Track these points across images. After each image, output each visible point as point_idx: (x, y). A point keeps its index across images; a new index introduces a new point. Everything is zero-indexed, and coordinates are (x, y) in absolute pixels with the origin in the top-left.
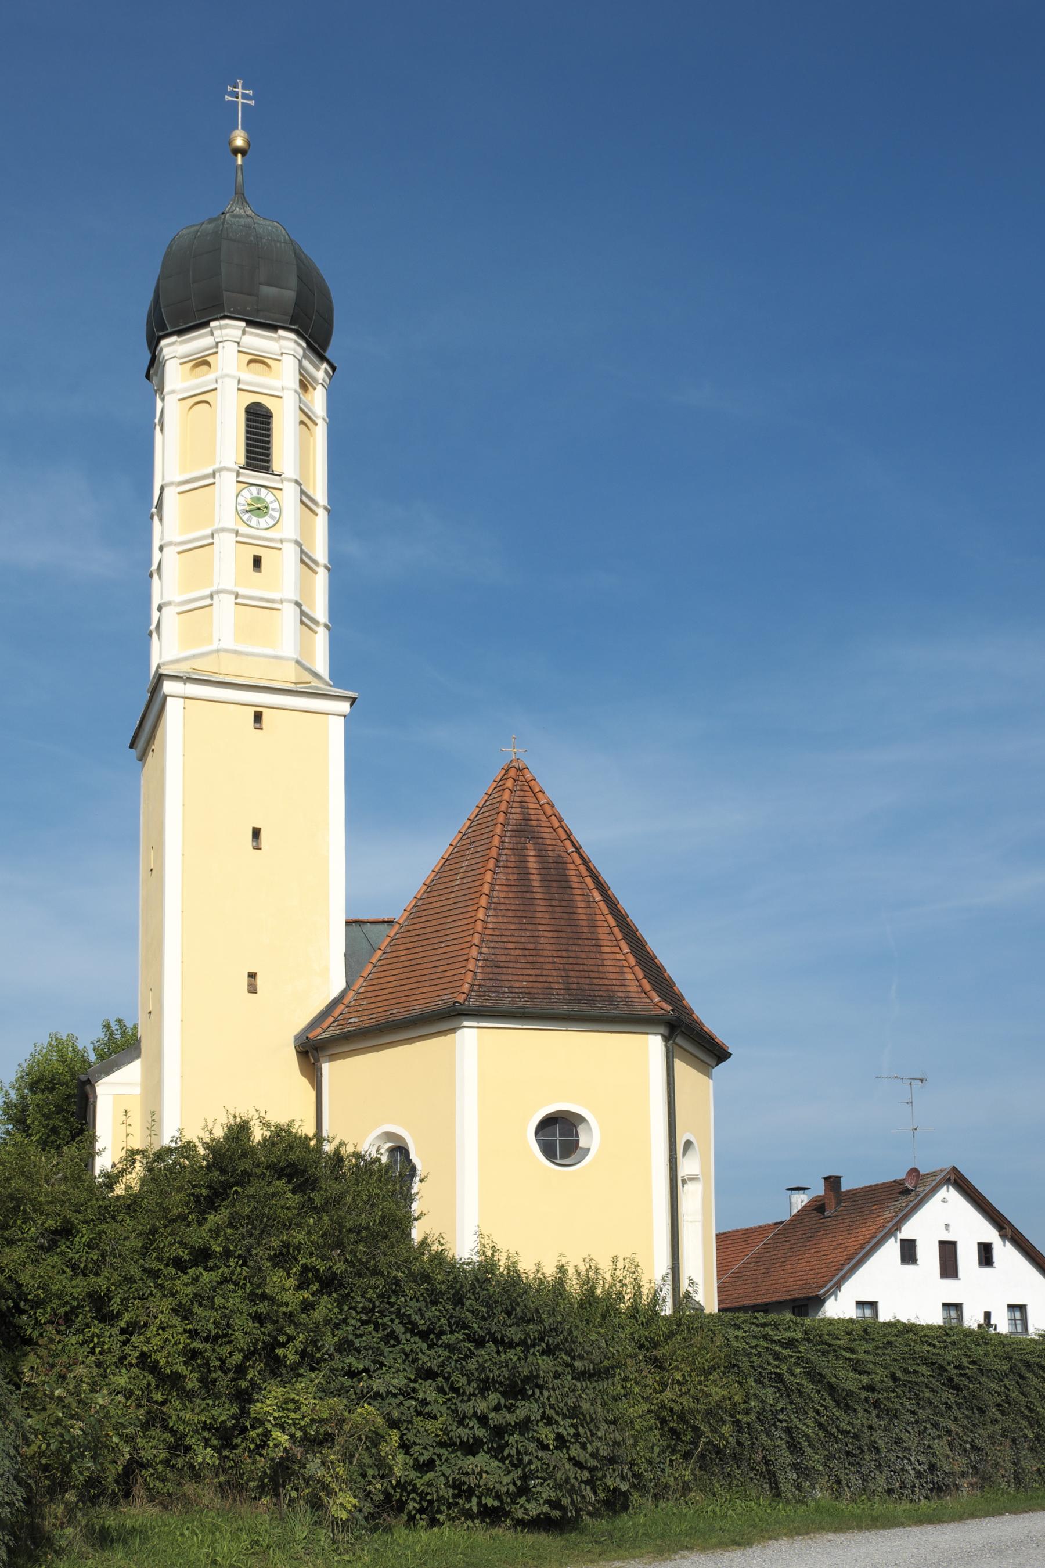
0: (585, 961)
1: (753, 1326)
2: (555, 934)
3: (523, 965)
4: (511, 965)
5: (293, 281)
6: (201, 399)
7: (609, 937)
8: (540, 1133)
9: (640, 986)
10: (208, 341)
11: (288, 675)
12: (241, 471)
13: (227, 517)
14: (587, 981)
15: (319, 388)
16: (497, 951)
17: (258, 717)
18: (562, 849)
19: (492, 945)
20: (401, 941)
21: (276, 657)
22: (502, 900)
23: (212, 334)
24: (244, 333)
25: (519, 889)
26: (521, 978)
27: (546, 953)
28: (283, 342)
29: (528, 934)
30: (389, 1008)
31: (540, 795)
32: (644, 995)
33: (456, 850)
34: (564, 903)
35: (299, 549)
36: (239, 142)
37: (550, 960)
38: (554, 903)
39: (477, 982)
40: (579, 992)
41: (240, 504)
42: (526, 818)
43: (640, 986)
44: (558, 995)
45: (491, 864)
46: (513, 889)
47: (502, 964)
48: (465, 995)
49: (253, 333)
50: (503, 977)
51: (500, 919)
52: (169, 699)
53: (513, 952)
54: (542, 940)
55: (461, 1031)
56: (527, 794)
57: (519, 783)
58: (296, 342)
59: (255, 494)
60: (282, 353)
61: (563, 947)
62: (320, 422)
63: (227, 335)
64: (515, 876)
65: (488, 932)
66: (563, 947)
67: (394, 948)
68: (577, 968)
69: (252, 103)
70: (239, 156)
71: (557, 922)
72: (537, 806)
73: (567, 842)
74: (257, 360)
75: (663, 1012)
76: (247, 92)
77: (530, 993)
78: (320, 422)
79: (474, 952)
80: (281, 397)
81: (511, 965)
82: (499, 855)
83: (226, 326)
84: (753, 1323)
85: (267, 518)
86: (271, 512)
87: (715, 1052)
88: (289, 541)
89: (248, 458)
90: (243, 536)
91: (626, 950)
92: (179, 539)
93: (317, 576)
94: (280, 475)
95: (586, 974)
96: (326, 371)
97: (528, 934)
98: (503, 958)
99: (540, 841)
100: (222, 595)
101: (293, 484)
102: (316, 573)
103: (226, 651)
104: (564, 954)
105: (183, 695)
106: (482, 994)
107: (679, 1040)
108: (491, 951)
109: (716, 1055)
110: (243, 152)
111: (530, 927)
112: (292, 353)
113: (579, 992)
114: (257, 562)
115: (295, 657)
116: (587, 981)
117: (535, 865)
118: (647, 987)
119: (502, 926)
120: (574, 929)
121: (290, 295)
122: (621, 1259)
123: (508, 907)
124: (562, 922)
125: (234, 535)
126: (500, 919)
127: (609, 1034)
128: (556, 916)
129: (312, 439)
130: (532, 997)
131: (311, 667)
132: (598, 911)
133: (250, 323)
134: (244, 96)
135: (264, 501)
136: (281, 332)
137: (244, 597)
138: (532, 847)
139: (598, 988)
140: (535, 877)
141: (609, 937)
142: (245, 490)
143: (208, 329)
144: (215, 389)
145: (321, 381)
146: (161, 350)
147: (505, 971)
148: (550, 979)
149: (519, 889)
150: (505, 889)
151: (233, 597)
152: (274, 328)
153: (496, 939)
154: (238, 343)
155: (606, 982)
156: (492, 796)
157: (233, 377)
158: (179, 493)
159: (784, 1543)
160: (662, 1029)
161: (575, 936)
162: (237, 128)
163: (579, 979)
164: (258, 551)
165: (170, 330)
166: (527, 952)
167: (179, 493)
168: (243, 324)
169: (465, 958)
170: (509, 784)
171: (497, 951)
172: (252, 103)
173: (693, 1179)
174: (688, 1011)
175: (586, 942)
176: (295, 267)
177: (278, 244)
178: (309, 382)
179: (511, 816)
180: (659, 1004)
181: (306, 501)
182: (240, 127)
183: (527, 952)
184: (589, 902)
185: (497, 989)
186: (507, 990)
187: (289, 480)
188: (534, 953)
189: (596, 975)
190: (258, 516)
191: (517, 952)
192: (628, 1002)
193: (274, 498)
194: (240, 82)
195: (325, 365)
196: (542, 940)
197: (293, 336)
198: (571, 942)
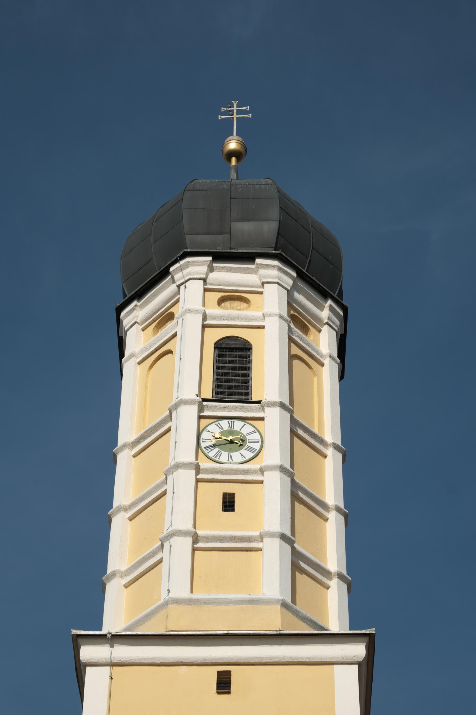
5: (275, 213)
12: (205, 403)
15: (325, 329)
21: (251, 602)
23: (174, 282)
24: (211, 269)
28: (262, 272)
35: (289, 480)
36: (233, 145)
41: (204, 440)
49: (223, 268)
58: (280, 269)
60: (263, 284)
62: (327, 361)
70: (234, 159)
78: (327, 361)
80: (263, 327)
83: (188, 263)
85: (243, 451)
86: (248, 444)
90: (207, 471)
92: (127, 502)
93: (328, 524)
96: (331, 309)
101: (277, 410)
102: (326, 520)
103: (177, 601)
105: (108, 661)
112: (276, 280)
115: (281, 598)
129: (315, 379)
135: (237, 433)
136: (258, 261)
137: (208, 539)
142: (213, 425)
143: (170, 276)
144: (175, 335)
145: (326, 321)
151: (189, 540)
154: (205, 280)
157: (197, 311)
159: (218, 416)
162: (232, 135)
164: (229, 488)
165: (128, 296)
168: (210, 258)
187: (272, 404)
193: (253, 429)
195: (330, 302)
197: (275, 263)
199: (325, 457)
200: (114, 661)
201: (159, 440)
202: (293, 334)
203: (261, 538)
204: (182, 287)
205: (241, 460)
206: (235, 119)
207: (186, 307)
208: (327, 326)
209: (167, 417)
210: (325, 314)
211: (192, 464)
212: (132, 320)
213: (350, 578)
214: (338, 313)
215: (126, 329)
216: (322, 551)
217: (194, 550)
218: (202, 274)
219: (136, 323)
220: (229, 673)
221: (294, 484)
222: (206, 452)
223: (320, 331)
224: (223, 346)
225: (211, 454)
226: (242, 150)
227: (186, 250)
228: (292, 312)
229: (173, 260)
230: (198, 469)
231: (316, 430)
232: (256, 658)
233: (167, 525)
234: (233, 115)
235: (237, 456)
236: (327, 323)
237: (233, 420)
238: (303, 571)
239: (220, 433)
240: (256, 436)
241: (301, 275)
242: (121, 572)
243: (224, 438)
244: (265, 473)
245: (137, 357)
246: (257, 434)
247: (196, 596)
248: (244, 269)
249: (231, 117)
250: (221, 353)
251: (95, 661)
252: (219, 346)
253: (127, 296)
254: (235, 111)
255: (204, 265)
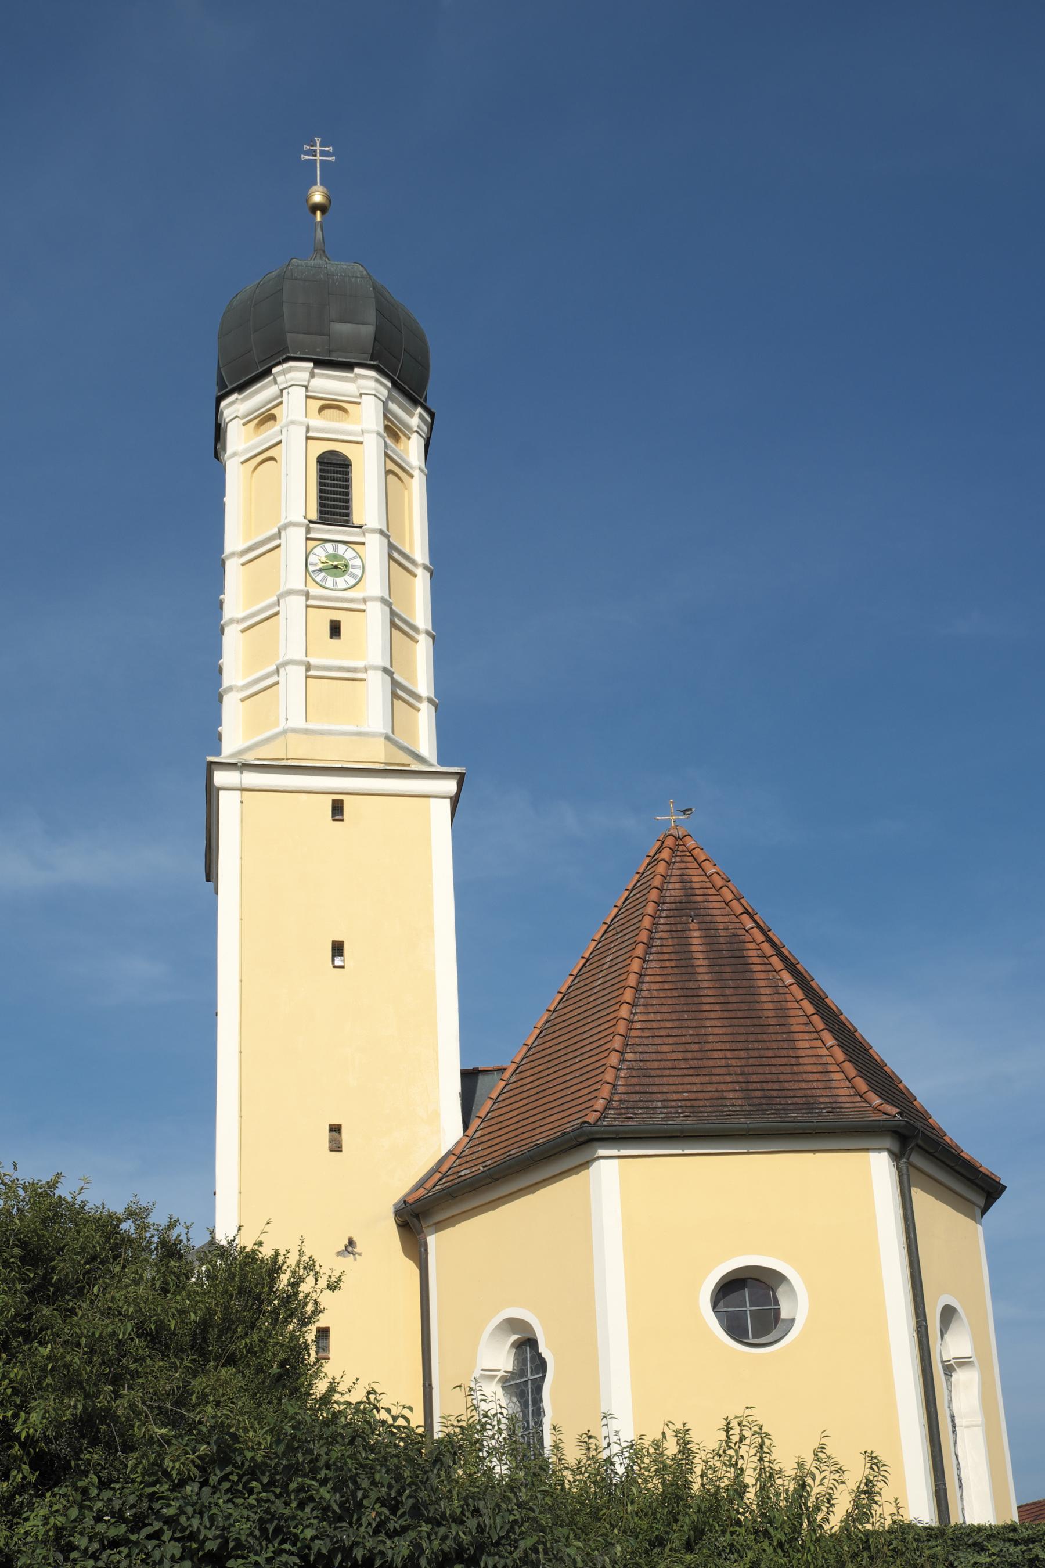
0: (773, 1061)
1: (1007, 1545)
2: (729, 1030)
3: (685, 1072)
4: (667, 1072)
5: (372, 316)
6: (265, 457)
7: (807, 1029)
8: (721, 1304)
9: (853, 1087)
10: (273, 390)
11: (376, 754)
12: (312, 525)
13: (296, 579)
14: (776, 1086)
15: (414, 436)
16: (647, 1057)
17: (338, 809)
18: (738, 926)
19: (639, 1049)
20: (528, 1066)
21: (360, 734)
22: (655, 993)
23: (275, 382)
24: (312, 375)
25: (678, 978)
26: (680, 1088)
27: (715, 1055)
28: (361, 382)
29: (691, 1032)
30: (507, 1149)
31: (706, 865)
32: (858, 1099)
33: (599, 945)
34: (741, 991)
35: (387, 610)
36: (318, 198)
37: (723, 1062)
38: (728, 992)
39: (616, 1097)
40: (763, 1101)
41: (312, 564)
42: (688, 892)
43: (853, 1087)
44: (734, 1106)
45: (640, 950)
46: (670, 978)
47: (654, 1073)
48: (598, 1114)
49: (323, 375)
50: (655, 1089)
51: (652, 1017)
52: (221, 793)
53: (669, 1056)
54: (711, 1038)
55: (596, 1164)
56: (689, 865)
57: (679, 853)
58: (377, 380)
59: (331, 551)
60: (361, 395)
61: (741, 1045)
62: (416, 473)
63: (292, 379)
64: (673, 964)
65: (633, 1033)
66: (741, 1045)
67: (520, 1076)
68: (760, 1070)
69: (333, 159)
70: (318, 213)
71: (732, 1014)
72: (704, 878)
73: (745, 917)
74: (331, 406)
75: (885, 1116)
76: (327, 149)
77: (693, 1107)
78: (416, 473)
79: (614, 1059)
80: (361, 443)
81: (667, 1072)
82: (651, 939)
83: (290, 370)
84: (1010, 1540)
85: (346, 577)
86: (351, 570)
87: (977, 1181)
88: (373, 599)
89: (321, 512)
90: (316, 598)
91: (831, 1042)
92: (241, 615)
94: (360, 527)
95: (775, 1078)
96: (421, 417)
97: (691, 1032)
98: (656, 1065)
99: (708, 919)
100: (289, 668)
101: (377, 536)
103: (295, 731)
104: (742, 1054)
105: (239, 786)
106: (623, 1111)
107: (916, 1159)
108: (638, 1057)
109: (982, 1189)
110: (323, 208)
111: (694, 1023)
112: (373, 392)
113: (763, 1101)
114: (335, 630)
116: (776, 1086)
117: (700, 948)
118: (862, 1085)
119: (655, 1025)
120: (756, 1021)
121: (367, 331)
122: (734, 1424)
123: (664, 1001)
124: (740, 1014)
125: (304, 598)
126: (652, 1017)
127: (811, 1155)
128: (730, 1007)
129: (406, 493)
130: (694, 1110)
131: (409, 747)
132: (789, 997)
133: (319, 363)
134: (323, 154)
135: (342, 558)
136: (357, 370)
137: (319, 668)
138: (696, 927)
139: (791, 1093)
140: (701, 962)
141: (807, 1029)
142: (319, 547)
143: (272, 377)
144: (280, 442)
145: (415, 429)
146: (222, 412)
147: (657, 1080)
148: (723, 1087)
149: (678, 978)
150: (659, 979)
151: (303, 668)
152: (348, 366)
153: (646, 1041)
154: (306, 387)
155: (804, 1085)
156: (645, 875)
157: (300, 423)
158: (243, 565)
160: (888, 1142)
161: (757, 1030)
163: (764, 1085)
164: (336, 615)
165: (230, 387)
166: (689, 1055)
167: (243, 565)
168: (311, 365)
169: (602, 1069)
170: (665, 854)
171: (647, 1057)
172: (333, 159)
173: (964, 1363)
174: (923, 1116)
175: (773, 1037)
176: (374, 300)
177: (353, 280)
178: (400, 430)
179: (668, 893)
180: (880, 1108)
181: (396, 556)
182: (319, 184)
183: (689, 1055)
184: (776, 987)
185: (645, 1104)
186: (659, 1104)
187: (373, 531)
188: (699, 1055)
189: (790, 1077)
190: (335, 576)
191: (674, 1056)
192: (834, 1108)
193: (355, 554)
194: (318, 141)
195: (419, 410)
196: (711, 1038)
197: (372, 373)
198: (752, 1038)
199: (415, 576)
200: (243, 787)
201: (267, 554)
202: (387, 449)
203: (365, 670)
204: (285, 392)
205: (346, 586)
206: (318, 161)
207: (289, 418)
208: (416, 434)
209: (275, 534)
210: (414, 422)
211: (302, 591)
212: (233, 413)
213: (437, 701)
214: (426, 420)
215: (227, 420)
216: (412, 675)
217: (307, 677)
218: (305, 381)
219: (237, 417)
220: (342, 801)
221: (393, 613)
222: (314, 576)
223: (409, 438)
224: (325, 461)
225: (318, 579)
226: (327, 203)
227: (289, 355)
228: (386, 423)
229: (276, 361)
230: (308, 595)
231: (407, 551)
232: (366, 789)
233: (282, 652)
234: (315, 156)
235: (341, 582)
236: (417, 432)
237: (337, 544)
238: (399, 698)
239: (326, 556)
240: (357, 562)
241: (394, 383)
242: (237, 687)
243: (331, 563)
244: (368, 603)
245: (240, 456)
246: (359, 559)
247: (311, 726)
248: (343, 377)
249: (314, 158)
250: (323, 468)
251: (226, 786)
252: (322, 460)
253: (227, 387)
254: (318, 151)
255: (306, 371)
